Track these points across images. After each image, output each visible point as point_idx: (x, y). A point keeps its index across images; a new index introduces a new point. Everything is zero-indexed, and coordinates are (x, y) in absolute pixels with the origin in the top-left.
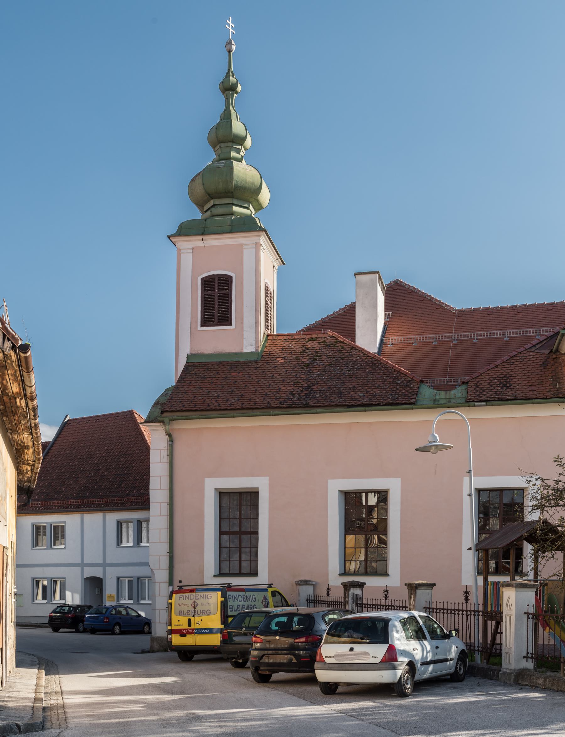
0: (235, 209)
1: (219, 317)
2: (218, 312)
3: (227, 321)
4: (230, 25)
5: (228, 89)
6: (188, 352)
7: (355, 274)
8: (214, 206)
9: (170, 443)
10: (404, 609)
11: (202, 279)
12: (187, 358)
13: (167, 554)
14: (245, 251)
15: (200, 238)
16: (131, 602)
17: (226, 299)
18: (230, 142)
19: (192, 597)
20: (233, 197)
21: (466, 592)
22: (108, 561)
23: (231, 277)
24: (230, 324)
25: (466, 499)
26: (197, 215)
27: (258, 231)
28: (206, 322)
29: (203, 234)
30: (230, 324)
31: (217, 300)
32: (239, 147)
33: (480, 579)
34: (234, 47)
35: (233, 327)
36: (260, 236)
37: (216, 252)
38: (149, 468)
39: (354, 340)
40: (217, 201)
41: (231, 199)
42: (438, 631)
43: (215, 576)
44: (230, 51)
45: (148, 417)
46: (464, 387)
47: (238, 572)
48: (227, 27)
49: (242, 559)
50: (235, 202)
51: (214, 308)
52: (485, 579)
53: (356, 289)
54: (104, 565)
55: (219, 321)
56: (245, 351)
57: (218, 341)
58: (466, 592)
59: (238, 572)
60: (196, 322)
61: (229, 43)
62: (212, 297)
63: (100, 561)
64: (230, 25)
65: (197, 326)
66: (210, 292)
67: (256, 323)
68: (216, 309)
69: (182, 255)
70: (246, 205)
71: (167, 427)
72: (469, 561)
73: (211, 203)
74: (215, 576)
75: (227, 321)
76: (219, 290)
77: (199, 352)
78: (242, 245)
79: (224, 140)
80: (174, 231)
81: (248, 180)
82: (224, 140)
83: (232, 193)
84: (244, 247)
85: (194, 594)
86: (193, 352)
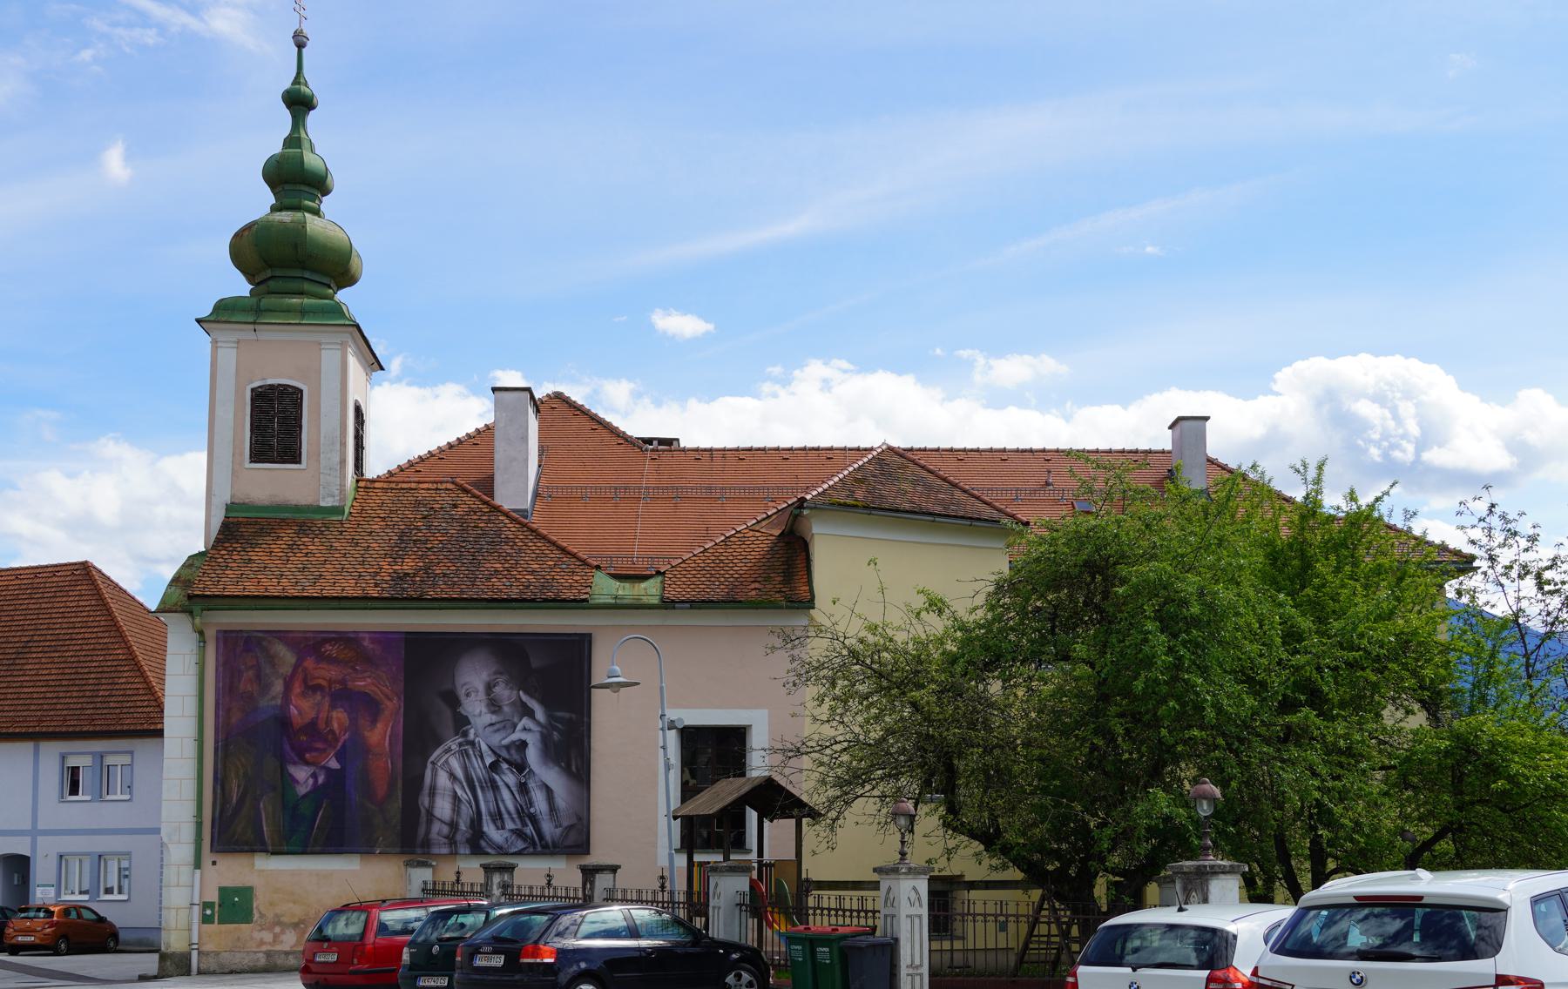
8: (272, 277)
10: (430, 887)
16: (86, 897)
17: (292, 425)
20: (304, 269)
21: (662, 877)
22: (41, 826)
23: (301, 391)
24: (299, 462)
25: (662, 822)
26: (240, 286)
30: (299, 462)
33: (681, 861)
35: (303, 466)
37: (279, 356)
39: (492, 495)
40: (278, 273)
42: (1210, 713)
45: (163, 601)
46: (660, 578)
52: (690, 859)
54: (34, 833)
57: (275, 484)
58: (662, 877)
60: (242, 454)
63: (27, 826)
71: (197, 620)
72: (667, 834)
73: (269, 273)
79: (295, 180)
80: (206, 311)
82: (295, 180)
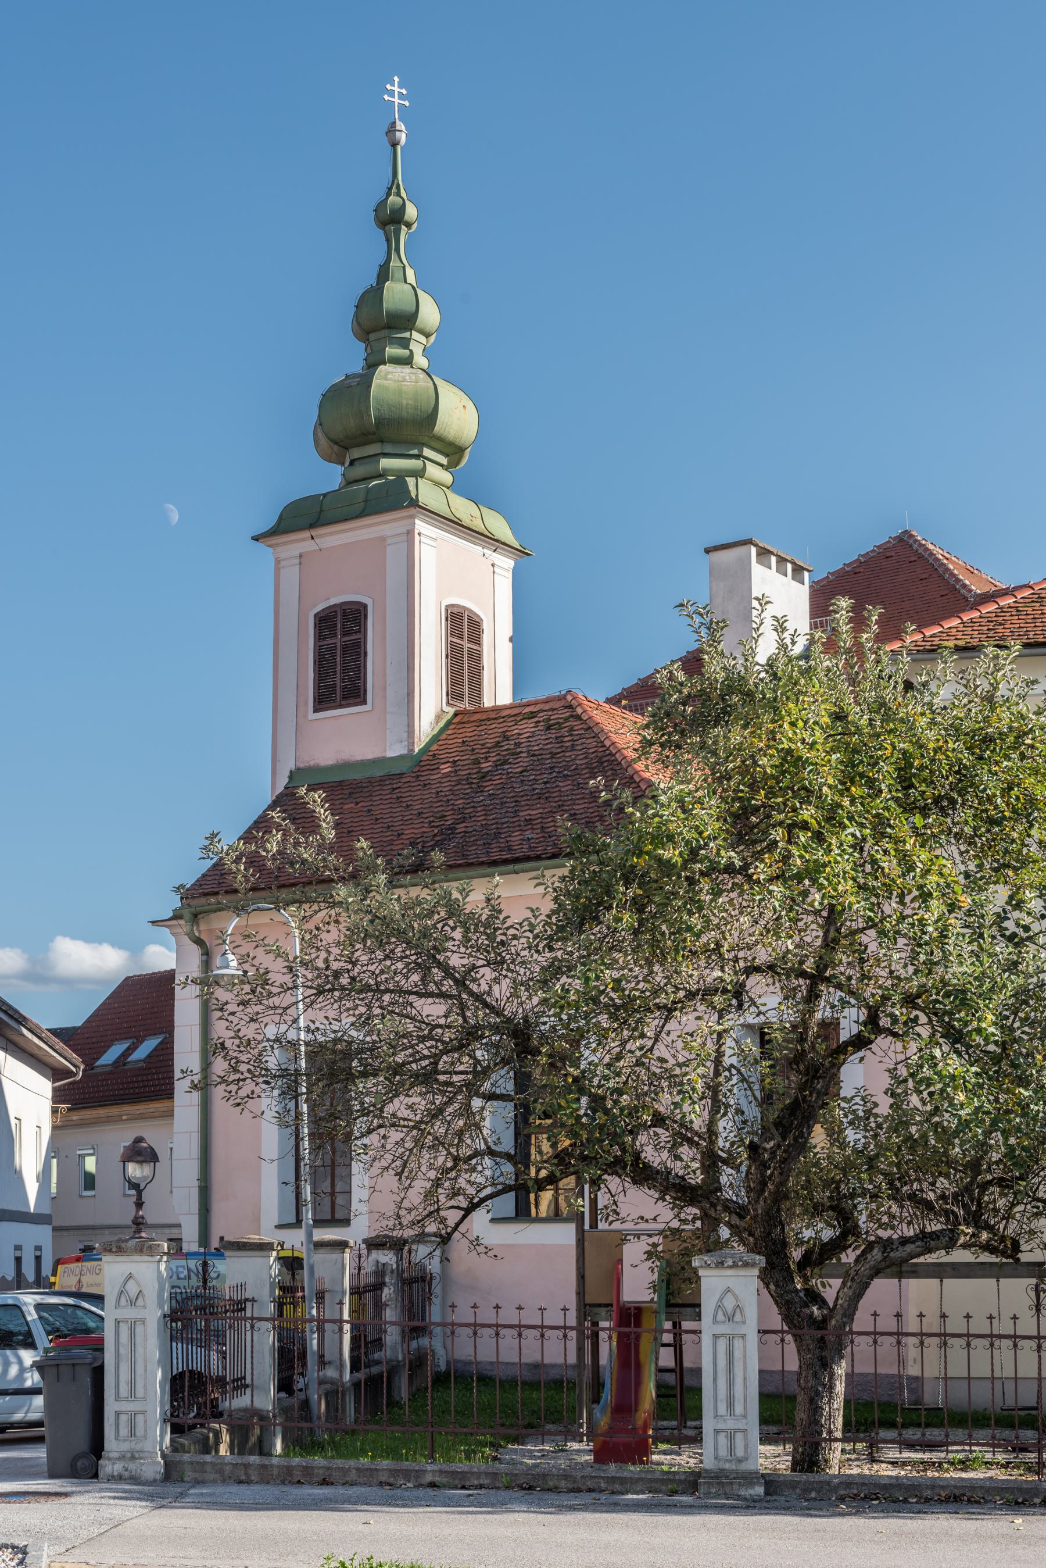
0: (385, 463)
1: (344, 688)
2: (343, 680)
3: (359, 696)
4: (396, 93)
5: (390, 220)
6: (291, 765)
7: (707, 551)
9: (205, 957)
11: (315, 615)
12: (290, 777)
13: (197, 1183)
14: (389, 549)
15: (306, 534)
17: (356, 651)
18: (384, 328)
19: (78, 1271)
27: (407, 507)
28: (324, 700)
29: (312, 526)
31: (341, 656)
32: (407, 335)
34: (403, 137)
36: (413, 517)
38: (173, 1010)
41: (379, 445)
43: (279, 1227)
44: (394, 144)
47: (329, 1217)
48: (386, 97)
49: (337, 1190)
50: (388, 449)
51: (335, 673)
53: (711, 582)
55: (344, 698)
56: (390, 754)
57: (348, 739)
59: (329, 1217)
61: (392, 129)
62: (332, 649)
64: (396, 93)
65: (307, 712)
66: (328, 641)
67: (408, 695)
68: (338, 675)
69: (282, 571)
70: (415, 452)
74: (279, 1227)
75: (359, 696)
76: (344, 635)
77: (312, 763)
78: (383, 539)
80: (269, 521)
81: (405, 402)
83: (374, 434)
84: (389, 541)
85: (80, 1264)
86: (302, 765)
